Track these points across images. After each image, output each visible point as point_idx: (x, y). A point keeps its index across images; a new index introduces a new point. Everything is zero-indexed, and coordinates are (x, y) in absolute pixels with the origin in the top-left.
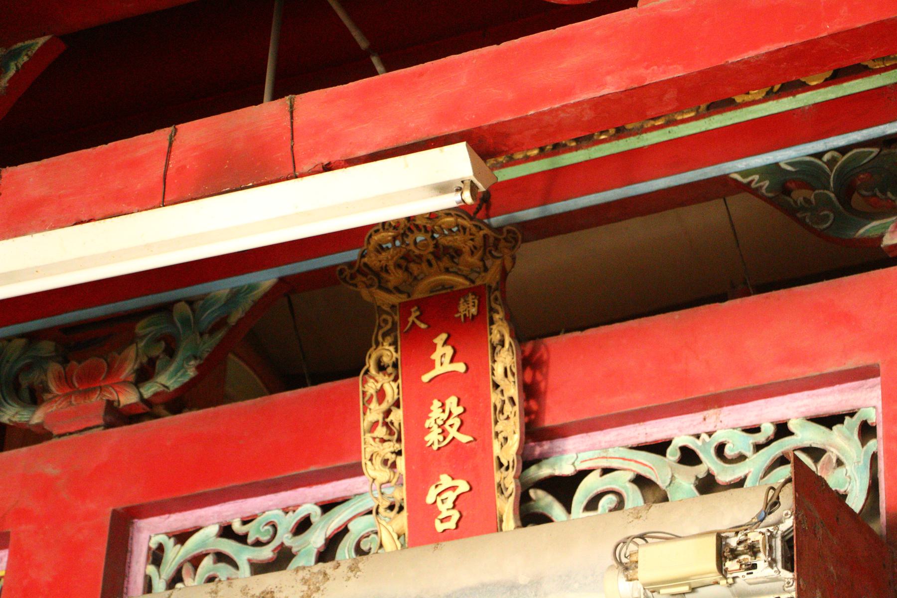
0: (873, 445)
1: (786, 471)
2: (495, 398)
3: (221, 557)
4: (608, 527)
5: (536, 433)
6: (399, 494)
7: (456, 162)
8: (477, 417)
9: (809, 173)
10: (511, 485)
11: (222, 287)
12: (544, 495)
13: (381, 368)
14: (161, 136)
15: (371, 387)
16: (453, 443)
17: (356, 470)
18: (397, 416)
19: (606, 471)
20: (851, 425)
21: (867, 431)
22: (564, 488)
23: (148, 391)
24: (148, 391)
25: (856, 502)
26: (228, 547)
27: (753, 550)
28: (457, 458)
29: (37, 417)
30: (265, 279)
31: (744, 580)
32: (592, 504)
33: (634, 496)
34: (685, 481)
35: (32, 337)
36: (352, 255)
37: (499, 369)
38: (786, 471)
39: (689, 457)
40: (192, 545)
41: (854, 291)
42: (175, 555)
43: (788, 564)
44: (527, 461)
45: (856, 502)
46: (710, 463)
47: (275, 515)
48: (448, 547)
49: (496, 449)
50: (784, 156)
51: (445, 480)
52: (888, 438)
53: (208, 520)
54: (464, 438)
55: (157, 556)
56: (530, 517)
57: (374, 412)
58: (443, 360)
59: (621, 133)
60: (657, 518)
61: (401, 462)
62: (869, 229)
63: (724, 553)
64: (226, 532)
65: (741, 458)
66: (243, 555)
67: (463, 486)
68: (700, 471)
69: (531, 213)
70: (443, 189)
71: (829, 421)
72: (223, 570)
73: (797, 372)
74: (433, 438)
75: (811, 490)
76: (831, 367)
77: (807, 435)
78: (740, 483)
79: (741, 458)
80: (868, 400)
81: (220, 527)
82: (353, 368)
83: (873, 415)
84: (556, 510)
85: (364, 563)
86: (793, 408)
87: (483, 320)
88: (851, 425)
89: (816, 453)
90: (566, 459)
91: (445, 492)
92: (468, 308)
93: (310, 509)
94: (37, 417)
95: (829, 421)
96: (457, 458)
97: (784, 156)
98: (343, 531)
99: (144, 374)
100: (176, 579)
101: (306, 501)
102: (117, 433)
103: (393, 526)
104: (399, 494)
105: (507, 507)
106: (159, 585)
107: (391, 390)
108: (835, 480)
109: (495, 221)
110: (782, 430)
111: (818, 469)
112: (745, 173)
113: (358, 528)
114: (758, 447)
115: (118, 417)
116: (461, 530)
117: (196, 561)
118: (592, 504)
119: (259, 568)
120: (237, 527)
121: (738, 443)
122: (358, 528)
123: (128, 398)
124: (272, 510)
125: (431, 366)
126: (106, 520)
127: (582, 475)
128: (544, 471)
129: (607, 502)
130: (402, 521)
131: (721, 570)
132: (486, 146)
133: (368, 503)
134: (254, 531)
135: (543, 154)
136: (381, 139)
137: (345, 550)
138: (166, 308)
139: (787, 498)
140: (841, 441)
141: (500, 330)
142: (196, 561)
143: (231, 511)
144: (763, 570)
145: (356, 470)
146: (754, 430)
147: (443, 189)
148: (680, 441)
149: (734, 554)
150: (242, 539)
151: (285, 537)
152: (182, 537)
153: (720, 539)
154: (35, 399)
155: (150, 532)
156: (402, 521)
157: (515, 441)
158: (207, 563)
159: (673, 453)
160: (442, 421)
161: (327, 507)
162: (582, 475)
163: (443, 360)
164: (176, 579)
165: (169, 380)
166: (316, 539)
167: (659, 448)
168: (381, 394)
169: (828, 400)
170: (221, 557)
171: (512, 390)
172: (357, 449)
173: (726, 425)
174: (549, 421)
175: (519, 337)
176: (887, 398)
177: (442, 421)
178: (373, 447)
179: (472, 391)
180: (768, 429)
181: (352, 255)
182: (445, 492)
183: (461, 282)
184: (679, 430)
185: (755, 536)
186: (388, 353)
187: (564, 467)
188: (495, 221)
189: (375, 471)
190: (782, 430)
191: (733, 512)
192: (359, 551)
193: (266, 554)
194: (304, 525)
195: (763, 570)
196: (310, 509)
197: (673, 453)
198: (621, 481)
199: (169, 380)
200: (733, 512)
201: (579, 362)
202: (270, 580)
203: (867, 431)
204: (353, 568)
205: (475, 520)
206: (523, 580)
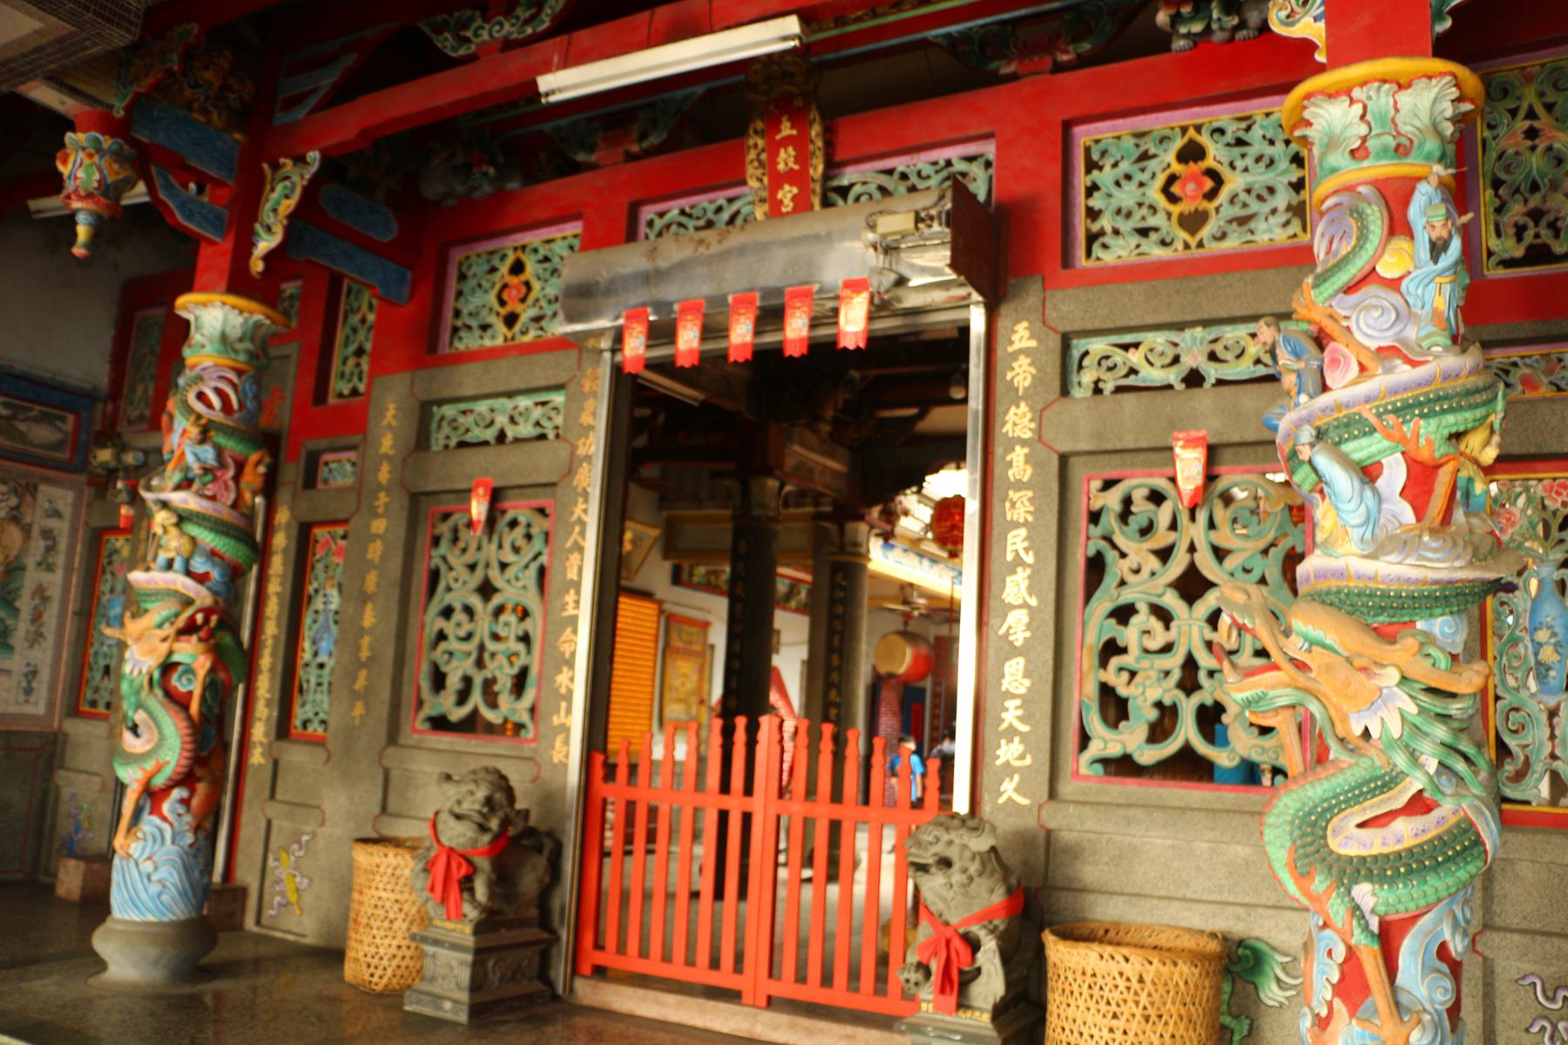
0: (991, 171)
1: (948, 183)
2: (811, 147)
3: (681, 225)
4: (866, 207)
5: (833, 166)
6: (765, 194)
7: (792, 25)
8: (803, 158)
9: (965, 37)
10: (818, 189)
11: (679, 94)
12: (834, 194)
13: (756, 132)
14: (646, 15)
15: (751, 142)
16: (623, 223)
17: (744, 183)
18: (764, 156)
19: (864, 183)
20: (981, 161)
21: (988, 164)
22: (844, 192)
23: (645, 145)
24: (645, 145)
25: (982, 197)
26: (684, 220)
27: (932, 218)
28: (791, 177)
29: (593, 158)
30: (700, 89)
31: (926, 231)
32: (857, 199)
33: (877, 195)
34: (902, 188)
35: (590, 120)
36: (741, 77)
37: (813, 133)
38: (948, 183)
39: (904, 176)
40: (667, 218)
41: (986, 97)
42: (659, 223)
43: (948, 225)
44: (827, 177)
45: (982, 197)
46: (914, 179)
47: (705, 204)
48: (787, 220)
49: (811, 172)
50: (954, 29)
51: (787, 187)
52: (998, 167)
53: (673, 209)
54: (796, 167)
55: (650, 224)
56: (827, 203)
57: (752, 155)
58: (787, 130)
59: (875, 15)
60: (888, 203)
61: (766, 180)
62: (993, 65)
63: (918, 219)
64: (683, 212)
65: (928, 177)
66: (691, 224)
67: (795, 190)
68: (909, 183)
69: (830, 56)
70: (785, 38)
71: (970, 159)
72: (682, 231)
73: (962, 135)
74: (781, 167)
75: (959, 186)
76: (973, 132)
77: (960, 166)
78: (928, 188)
79: (928, 177)
80: (989, 149)
81: (177, 386)
82: (742, 133)
83: (991, 156)
84: (840, 202)
85: (747, 227)
86: (953, 153)
87: (804, 111)
88: (981, 161)
89: (964, 175)
90: (848, 176)
91: (787, 193)
92: (799, 103)
93: (722, 202)
94: (593, 158)
95: (970, 159)
96: (791, 177)
97: (954, 29)
98: (737, 213)
99: (643, 136)
100: (660, 234)
101: (720, 198)
102: (633, 164)
103: (760, 212)
104: (765, 194)
105: (816, 201)
106: (652, 237)
107: (761, 143)
108: (972, 187)
109: (814, 59)
110: (949, 163)
111: (965, 182)
112: (936, 37)
113: (745, 210)
114: (937, 172)
115: (630, 157)
116: (795, 210)
117: (668, 226)
118: (857, 199)
119: (697, 229)
120: (688, 210)
121: (927, 170)
122: (745, 210)
123: (635, 148)
124: (704, 202)
125: (779, 131)
126: (626, 206)
127: (852, 185)
128: (835, 183)
129: (864, 198)
130: (766, 207)
131: (917, 228)
132: (806, 18)
133: (750, 198)
134: (696, 212)
135: (837, 26)
136: (755, 13)
137: (739, 221)
138: (652, 105)
139: (949, 195)
140: (976, 169)
141: (814, 114)
142: (668, 226)
143: (685, 203)
144: (936, 227)
145: (744, 183)
146: (935, 163)
147: (785, 38)
148: (901, 168)
149: (923, 220)
150: (690, 216)
151: (710, 215)
152: (661, 215)
153: (917, 214)
154: (591, 149)
155: (648, 213)
156: (766, 207)
157: (821, 168)
158: (674, 228)
159: (896, 176)
160: (786, 159)
161: (731, 200)
162: (852, 185)
163: (787, 130)
164: (660, 234)
165: (654, 140)
166: (725, 216)
167: (890, 172)
168: (756, 146)
169: (971, 149)
170: (681, 225)
171: (820, 143)
172: (743, 172)
173: (922, 161)
174: (839, 157)
175: (824, 117)
176: (999, 149)
177: (786, 159)
178: (752, 171)
179: (800, 143)
180: (942, 163)
181: (741, 77)
182: (787, 193)
183: (794, 89)
184: (900, 163)
185: (933, 212)
186: (760, 125)
187: (845, 182)
188: (814, 59)
189: (753, 183)
190: (949, 163)
191: (923, 201)
192: (745, 221)
193: (702, 223)
194: (719, 210)
195: (936, 227)
196: (722, 202)
197: (896, 176)
198: (872, 188)
199: (654, 140)
200: (923, 201)
201: (851, 133)
202: (703, 234)
203: (988, 164)
204: (742, 228)
205: (802, 205)
206: (823, 233)
